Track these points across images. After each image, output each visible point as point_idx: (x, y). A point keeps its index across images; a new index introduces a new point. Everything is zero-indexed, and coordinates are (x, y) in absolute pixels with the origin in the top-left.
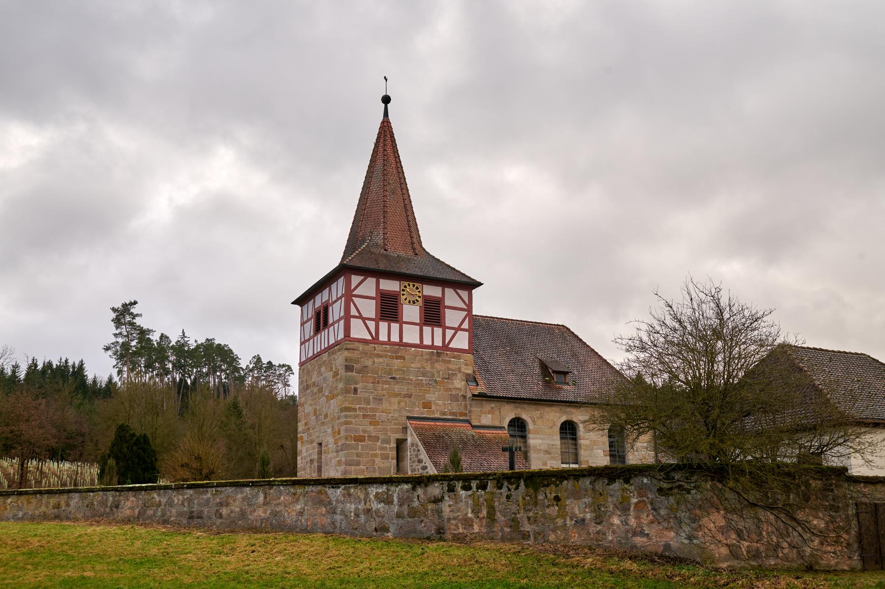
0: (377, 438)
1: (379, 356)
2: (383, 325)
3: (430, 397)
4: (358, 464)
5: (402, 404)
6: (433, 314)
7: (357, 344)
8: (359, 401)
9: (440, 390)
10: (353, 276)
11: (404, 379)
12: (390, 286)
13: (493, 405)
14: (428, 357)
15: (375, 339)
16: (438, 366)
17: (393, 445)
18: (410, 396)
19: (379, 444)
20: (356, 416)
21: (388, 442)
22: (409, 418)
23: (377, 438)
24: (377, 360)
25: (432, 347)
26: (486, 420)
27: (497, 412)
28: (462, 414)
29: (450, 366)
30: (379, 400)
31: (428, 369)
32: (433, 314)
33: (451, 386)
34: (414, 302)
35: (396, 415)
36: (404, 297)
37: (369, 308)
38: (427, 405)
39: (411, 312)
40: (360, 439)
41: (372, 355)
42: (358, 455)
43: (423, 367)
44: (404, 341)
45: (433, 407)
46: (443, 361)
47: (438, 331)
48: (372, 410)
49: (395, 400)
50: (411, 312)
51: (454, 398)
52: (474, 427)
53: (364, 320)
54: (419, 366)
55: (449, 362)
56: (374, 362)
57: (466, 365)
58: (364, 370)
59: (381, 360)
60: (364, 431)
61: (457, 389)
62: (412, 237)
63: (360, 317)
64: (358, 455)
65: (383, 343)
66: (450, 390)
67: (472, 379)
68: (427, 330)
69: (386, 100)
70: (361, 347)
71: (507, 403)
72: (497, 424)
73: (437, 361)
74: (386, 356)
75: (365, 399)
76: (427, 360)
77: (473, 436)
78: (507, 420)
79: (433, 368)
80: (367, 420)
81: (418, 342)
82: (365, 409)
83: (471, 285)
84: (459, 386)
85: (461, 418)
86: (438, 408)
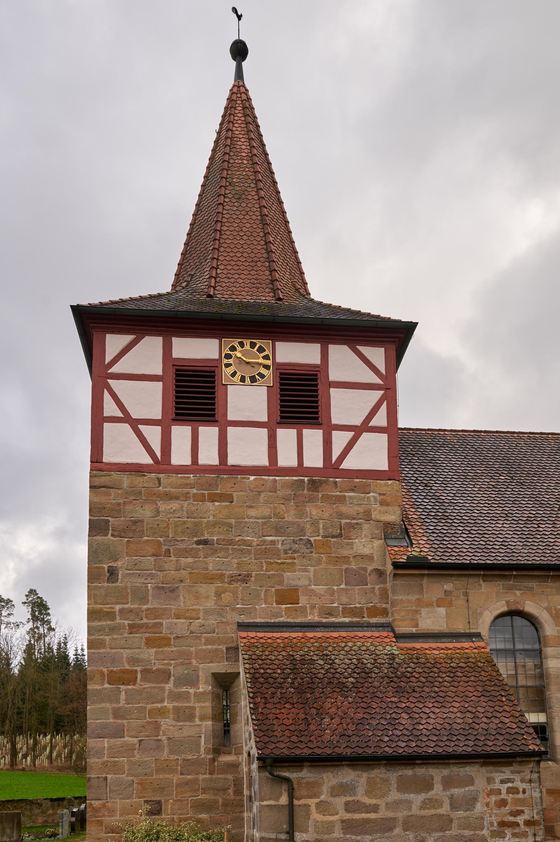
0: (165, 675)
1: (168, 497)
2: (181, 434)
3: (293, 578)
4: (119, 733)
5: (227, 597)
6: (299, 400)
7: (115, 475)
8: (122, 597)
9: (319, 562)
10: (108, 336)
11: (231, 542)
12: (298, 353)
13: (448, 586)
14: (289, 492)
15: (162, 463)
16: (312, 510)
17: (205, 687)
18: (246, 578)
19: (169, 686)
20: (113, 629)
21: (193, 681)
22: (242, 626)
23: (165, 675)
24: (163, 506)
25: (301, 469)
26: (433, 620)
27: (460, 602)
28: (374, 611)
29: (344, 509)
30: (169, 590)
31: (290, 517)
32: (299, 400)
33: (345, 552)
34: (253, 379)
35: (212, 621)
36: (228, 371)
37: (147, 401)
38: (288, 596)
39: (246, 400)
40: (128, 678)
41: (152, 497)
42: (117, 714)
43: (276, 515)
44: (232, 460)
45: (303, 600)
46: (327, 498)
47: (313, 437)
48: (154, 613)
49: (208, 590)
50: (246, 400)
51: (356, 578)
52: (399, 637)
53: (135, 424)
54: (266, 512)
55: (341, 500)
56: (158, 512)
57: (383, 503)
58: (134, 528)
59: (174, 505)
60: (133, 661)
61: (363, 557)
62: (272, 271)
63: (126, 418)
64: (117, 714)
65: (181, 470)
66: (346, 559)
67: (388, 532)
68: (286, 436)
69: (239, 51)
70: (126, 480)
71: (485, 578)
72: (460, 627)
73: (311, 500)
74: (186, 497)
75: (135, 590)
76: (287, 499)
77: (393, 657)
78: (488, 617)
79: (301, 514)
80: (140, 637)
81: (265, 462)
82: (137, 613)
83: (395, 335)
84: (367, 551)
85: (374, 620)
86: (315, 600)
